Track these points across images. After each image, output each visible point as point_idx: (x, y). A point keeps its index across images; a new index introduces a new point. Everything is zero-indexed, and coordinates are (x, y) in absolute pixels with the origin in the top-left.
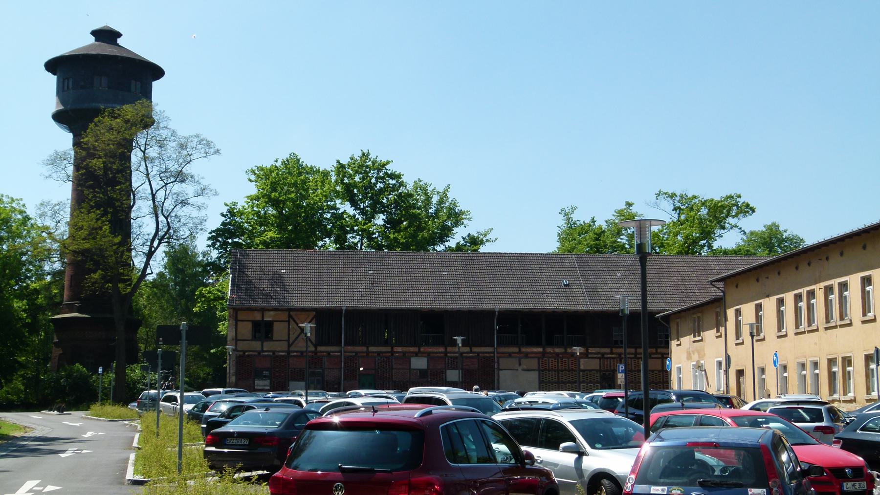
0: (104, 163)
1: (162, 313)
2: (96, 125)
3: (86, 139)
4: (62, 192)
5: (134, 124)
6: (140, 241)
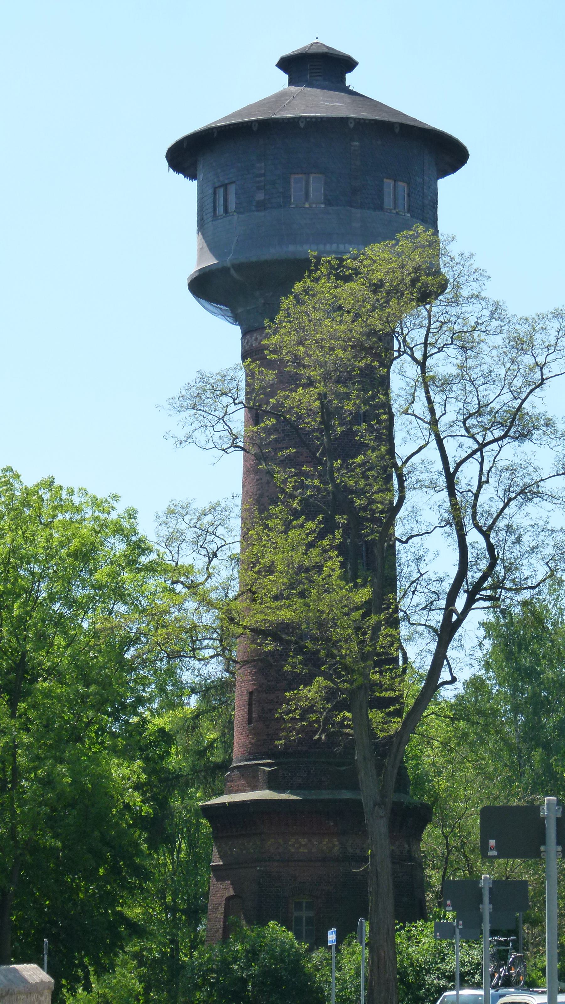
0: (322, 397)
1: (482, 786)
2: (299, 301)
3: (274, 340)
4: (220, 479)
5: (396, 292)
6: (420, 599)
